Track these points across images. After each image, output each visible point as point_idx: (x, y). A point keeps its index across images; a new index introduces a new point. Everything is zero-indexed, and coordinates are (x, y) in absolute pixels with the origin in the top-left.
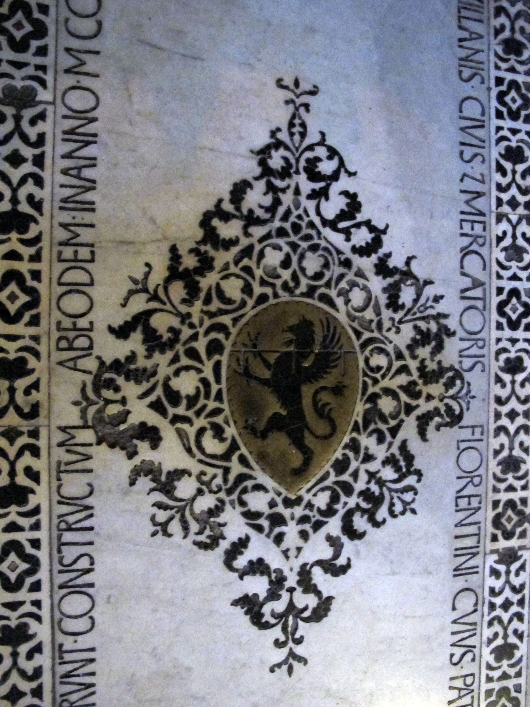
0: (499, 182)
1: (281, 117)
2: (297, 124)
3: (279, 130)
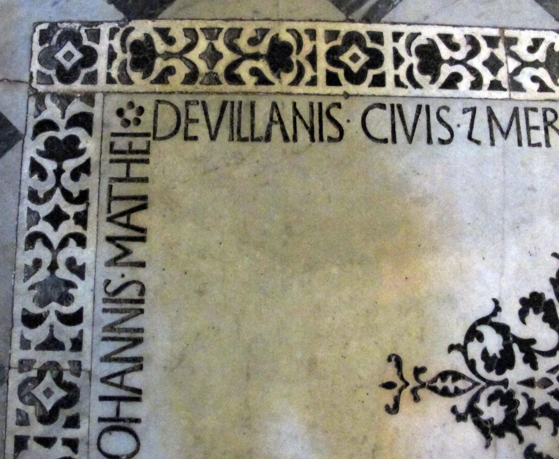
0: (469, 85)
1: (437, 407)
2: (443, 384)
3: (454, 410)
